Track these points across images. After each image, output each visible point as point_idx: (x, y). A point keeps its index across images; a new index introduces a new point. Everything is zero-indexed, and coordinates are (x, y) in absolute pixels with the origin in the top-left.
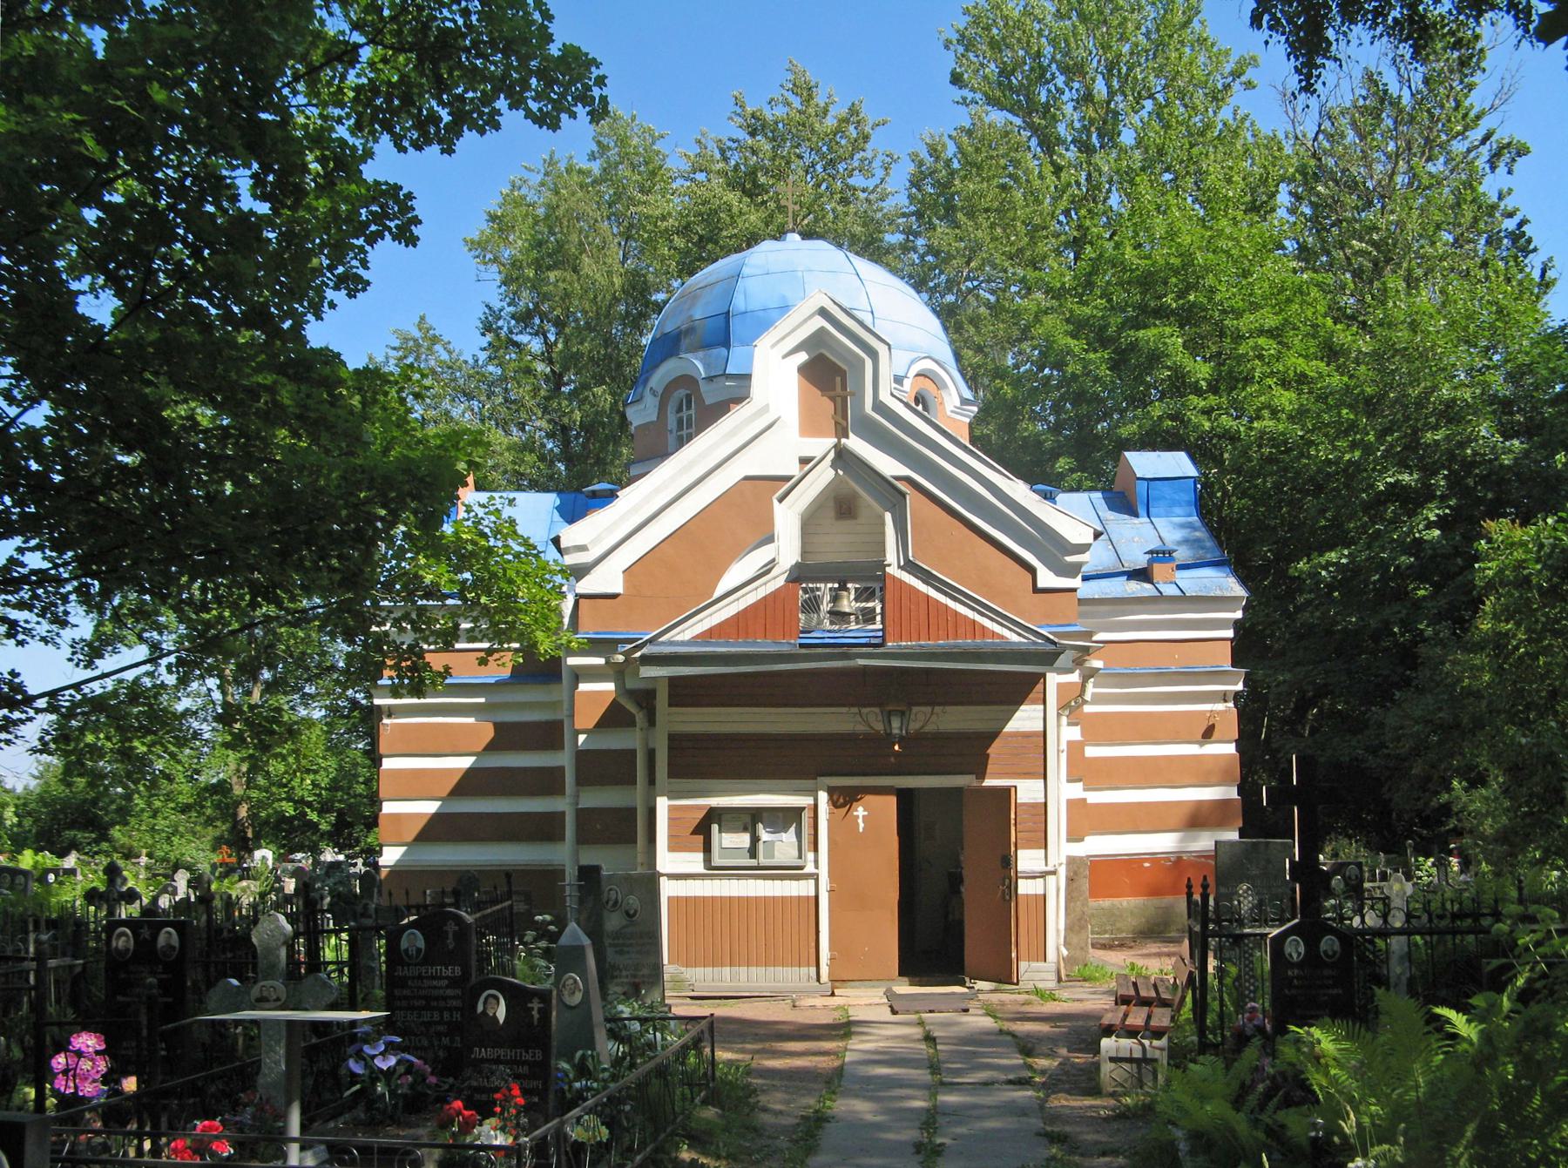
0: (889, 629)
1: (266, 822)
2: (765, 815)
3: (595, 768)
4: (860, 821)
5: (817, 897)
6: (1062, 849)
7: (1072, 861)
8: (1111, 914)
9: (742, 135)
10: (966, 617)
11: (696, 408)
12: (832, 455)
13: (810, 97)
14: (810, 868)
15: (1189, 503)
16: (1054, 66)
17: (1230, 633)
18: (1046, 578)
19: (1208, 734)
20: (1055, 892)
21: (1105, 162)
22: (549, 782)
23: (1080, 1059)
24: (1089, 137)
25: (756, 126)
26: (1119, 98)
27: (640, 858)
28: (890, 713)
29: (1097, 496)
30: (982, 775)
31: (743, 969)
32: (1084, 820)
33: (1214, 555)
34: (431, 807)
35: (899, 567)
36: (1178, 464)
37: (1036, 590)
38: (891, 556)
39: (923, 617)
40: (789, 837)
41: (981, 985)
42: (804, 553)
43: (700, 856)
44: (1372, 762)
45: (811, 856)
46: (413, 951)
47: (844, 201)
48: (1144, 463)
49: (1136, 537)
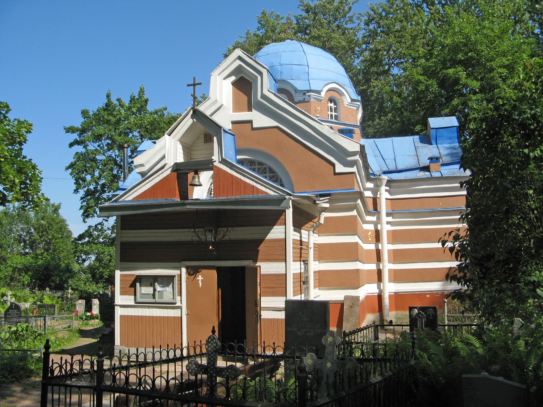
2: (159, 279)
4: (200, 282)
5: (181, 317)
9: (304, 14)
10: (249, 184)
12: (191, 112)
14: (178, 304)
18: (340, 168)
35: (219, 162)
37: (335, 174)
38: (215, 157)
40: (169, 289)
43: (133, 297)
48: (434, 122)
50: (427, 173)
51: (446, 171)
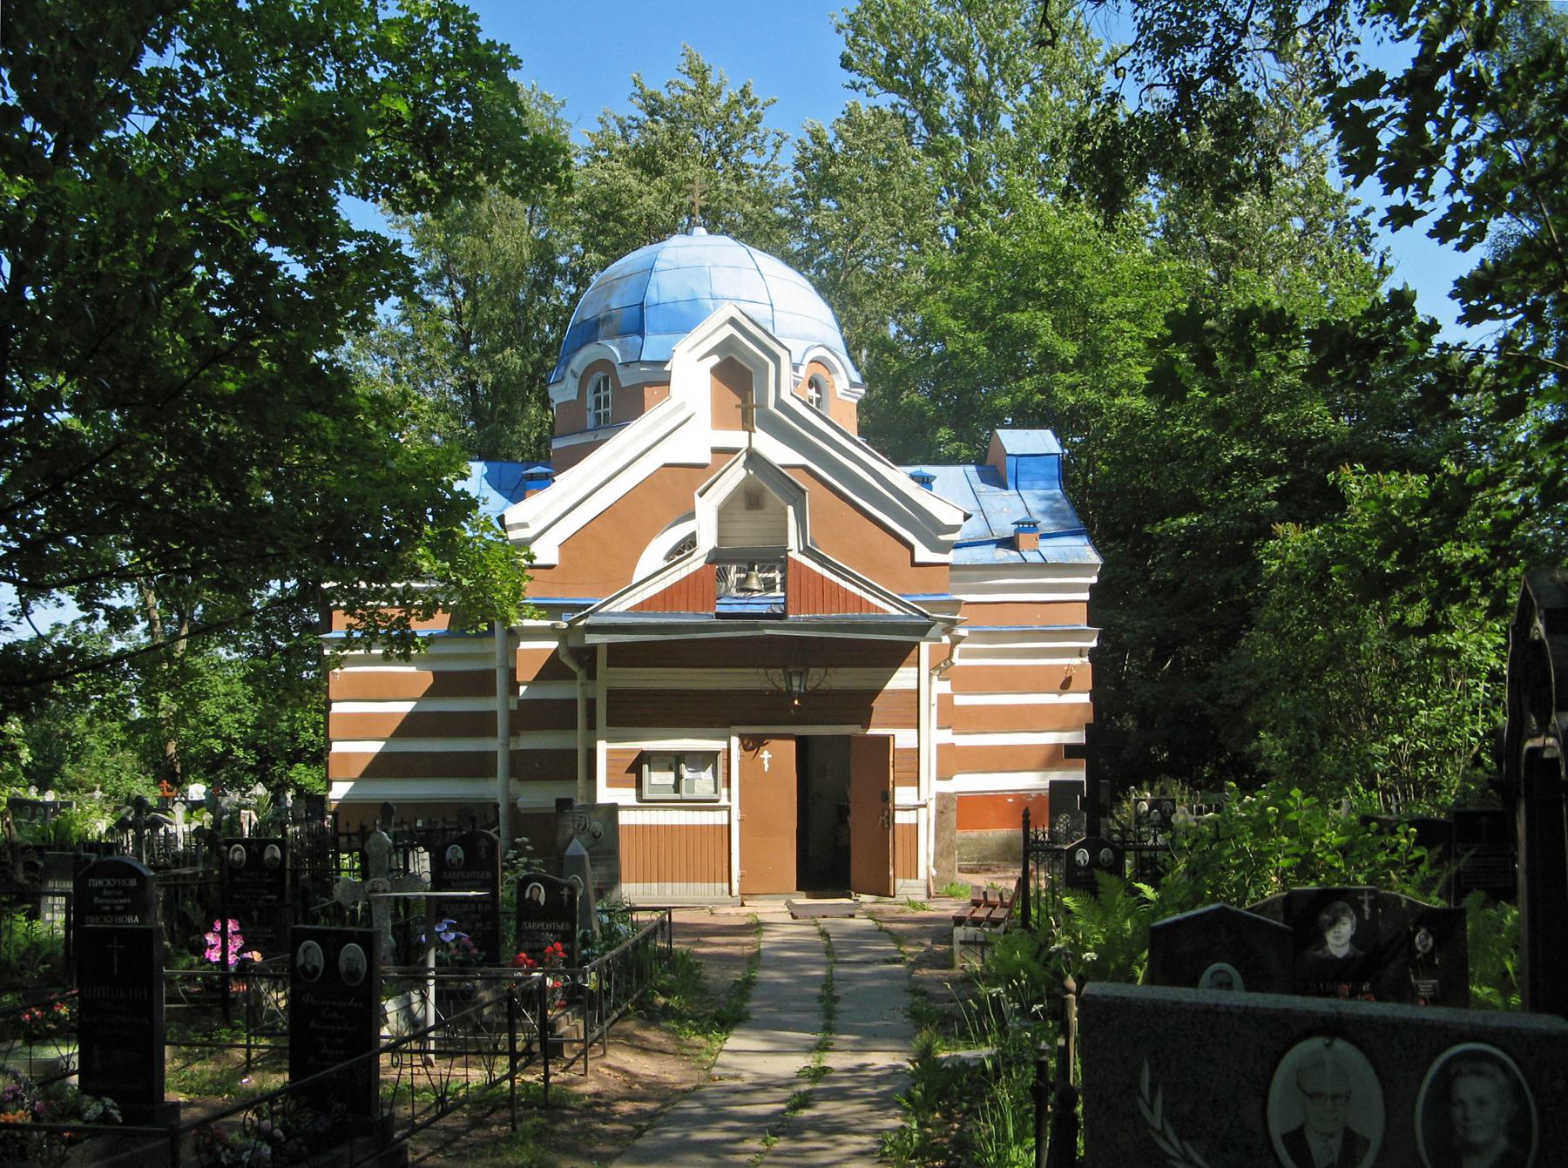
0: (790, 604)
1: (194, 758)
3: (529, 716)
6: (932, 785)
7: (941, 797)
8: (977, 842)
9: (642, 115)
11: (620, 399)
13: (704, 79)
14: (724, 802)
15: (1048, 478)
16: (938, 52)
17: (1086, 596)
18: (923, 554)
19: (1066, 686)
20: (925, 822)
21: (981, 147)
22: (481, 724)
23: (939, 948)
24: (971, 118)
25: (654, 108)
26: (998, 83)
27: (581, 792)
28: (790, 675)
29: (971, 469)
30: (867, 726)
31: (669, 885)
32: (952, 762)
33: (1075, 523)
34: (375, 747)
36: (1043, 441)
37: (914, 564)
38: (793, 543)
39: (819, 593)
40: (707, 775)
41: (864, 898)
42: (720, 538)
43: (633, 791)
44: (1210, 710)
45: (724, 791)
46: (455, 860)
47: (738, 179)
48: (1015, 440)
49: (1007, 508)
50: (1014, 553)
51: (1054, 549)
